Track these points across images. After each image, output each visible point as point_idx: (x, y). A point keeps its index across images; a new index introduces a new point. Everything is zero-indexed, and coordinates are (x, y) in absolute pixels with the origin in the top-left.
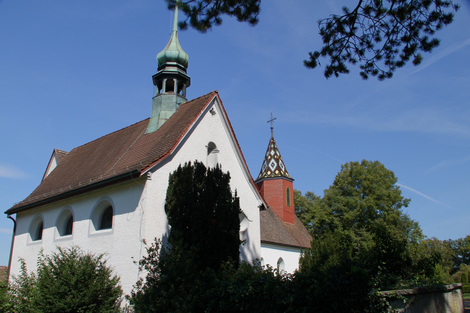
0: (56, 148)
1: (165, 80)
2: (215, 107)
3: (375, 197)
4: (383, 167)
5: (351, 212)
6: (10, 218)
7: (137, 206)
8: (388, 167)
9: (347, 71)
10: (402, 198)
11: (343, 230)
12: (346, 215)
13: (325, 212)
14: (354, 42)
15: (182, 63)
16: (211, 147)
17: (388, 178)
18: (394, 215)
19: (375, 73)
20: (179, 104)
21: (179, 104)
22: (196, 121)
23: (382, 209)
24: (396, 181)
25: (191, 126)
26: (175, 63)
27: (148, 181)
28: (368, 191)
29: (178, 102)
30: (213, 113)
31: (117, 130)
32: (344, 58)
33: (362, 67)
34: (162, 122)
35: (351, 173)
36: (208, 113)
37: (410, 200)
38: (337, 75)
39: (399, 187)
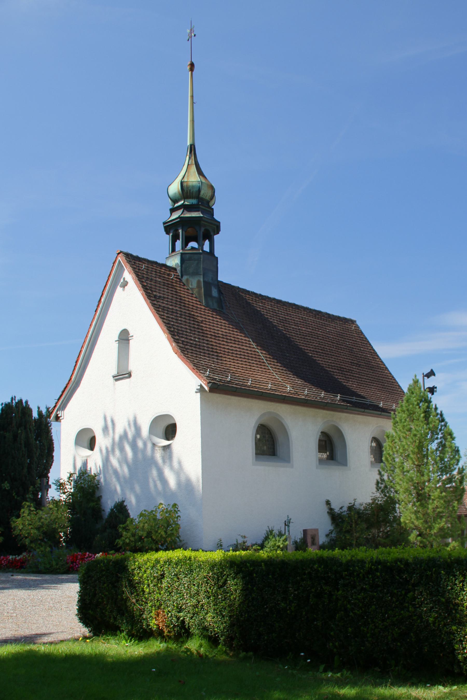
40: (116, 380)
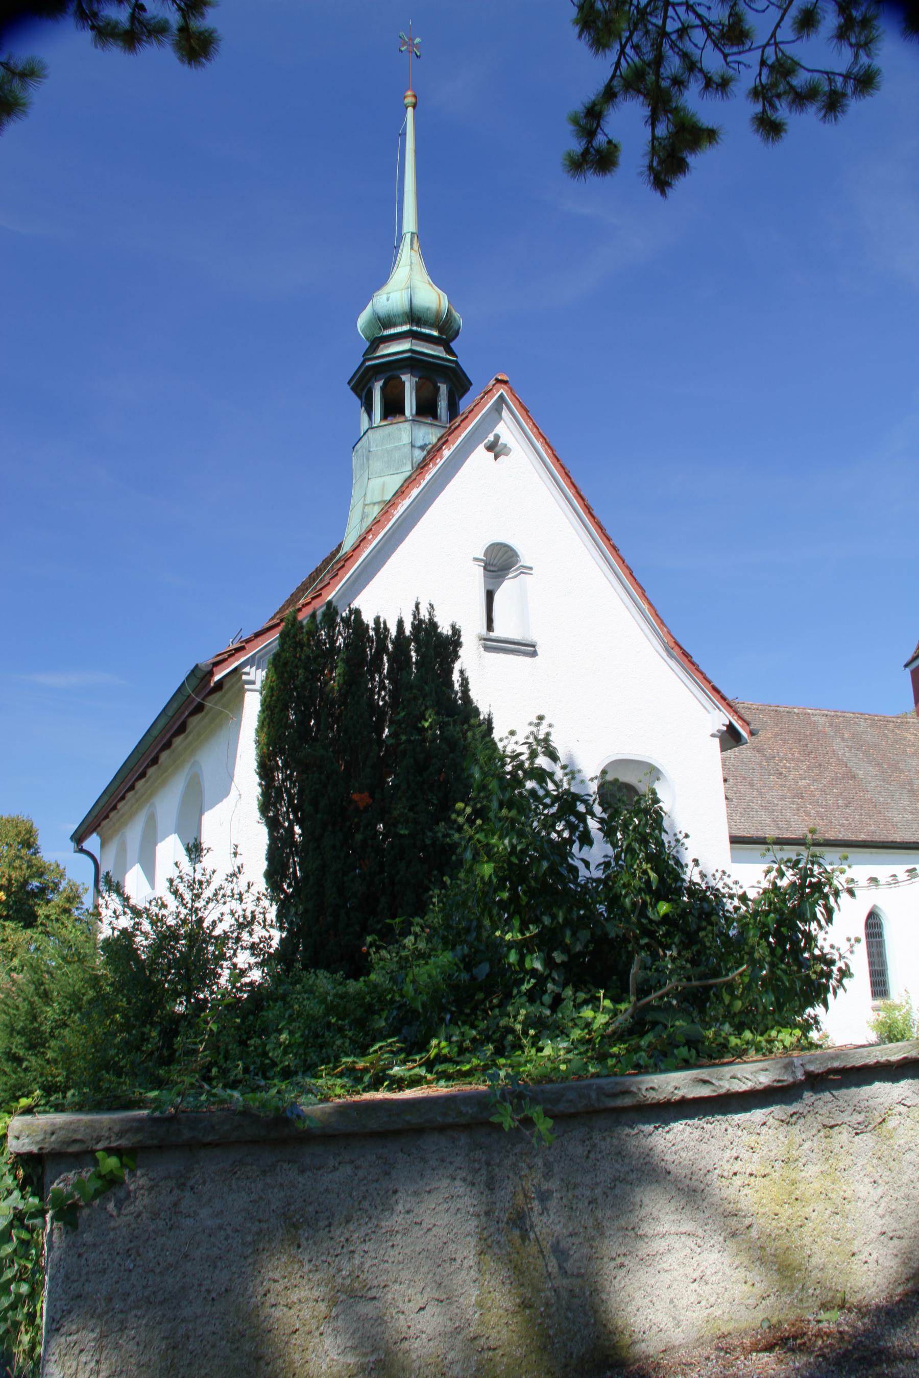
6: (82, 851)
9: (711, 135)
16: (500, 563)
19: (802, 98)
20: (422, 448)
21: (422, 448)
22: (423, 483)
26: (406, 328)
29: (419, 443)
36: (480, 454)
40: (487, 649)
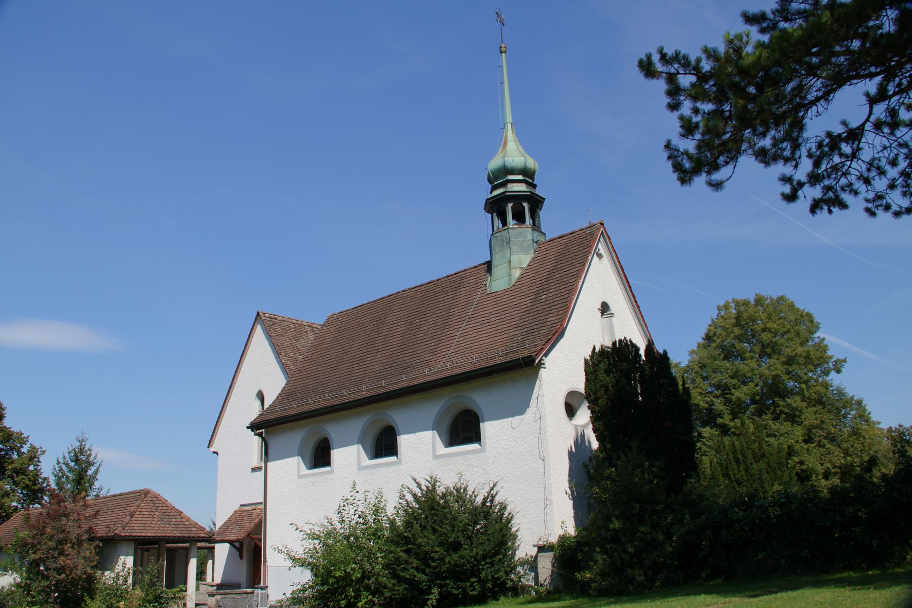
0: (261, 311)
1: (510, 205)
2: (602, 248)
3: (784, 359)
4: (792, 305)
5: (744, 388)
7: (527, 406)
8: (801, 304)
10: (831, 357)
11: (733, 419)
12: (737, 394)
13: (698, 390)
14: (857, 167)
15: (528, 175)
17: (808, 322)
18: (818, 388)
19: (887, 207)
20: (536, 242)
21: (536, 242)
23: (797, 378)
24: (818, 328)
25: (581, 281)
26: (520, 177)
27: (542, 371)
28: (768, 350)
30: (600, 256)
31: (420, 284)
32: (843, 189)
33: (867, 201)
34: (517, 274)
35: (738, 318)
37: (845, 361)
38: (830, 212)
39: (824, 339)
